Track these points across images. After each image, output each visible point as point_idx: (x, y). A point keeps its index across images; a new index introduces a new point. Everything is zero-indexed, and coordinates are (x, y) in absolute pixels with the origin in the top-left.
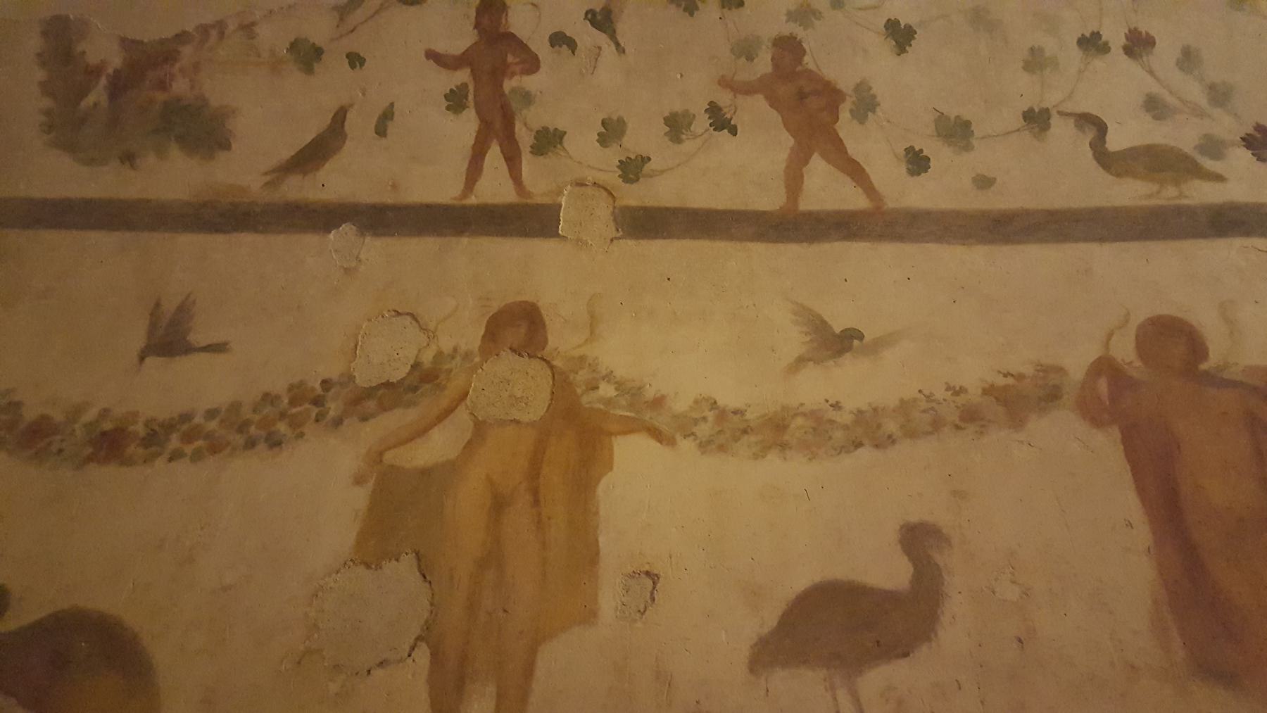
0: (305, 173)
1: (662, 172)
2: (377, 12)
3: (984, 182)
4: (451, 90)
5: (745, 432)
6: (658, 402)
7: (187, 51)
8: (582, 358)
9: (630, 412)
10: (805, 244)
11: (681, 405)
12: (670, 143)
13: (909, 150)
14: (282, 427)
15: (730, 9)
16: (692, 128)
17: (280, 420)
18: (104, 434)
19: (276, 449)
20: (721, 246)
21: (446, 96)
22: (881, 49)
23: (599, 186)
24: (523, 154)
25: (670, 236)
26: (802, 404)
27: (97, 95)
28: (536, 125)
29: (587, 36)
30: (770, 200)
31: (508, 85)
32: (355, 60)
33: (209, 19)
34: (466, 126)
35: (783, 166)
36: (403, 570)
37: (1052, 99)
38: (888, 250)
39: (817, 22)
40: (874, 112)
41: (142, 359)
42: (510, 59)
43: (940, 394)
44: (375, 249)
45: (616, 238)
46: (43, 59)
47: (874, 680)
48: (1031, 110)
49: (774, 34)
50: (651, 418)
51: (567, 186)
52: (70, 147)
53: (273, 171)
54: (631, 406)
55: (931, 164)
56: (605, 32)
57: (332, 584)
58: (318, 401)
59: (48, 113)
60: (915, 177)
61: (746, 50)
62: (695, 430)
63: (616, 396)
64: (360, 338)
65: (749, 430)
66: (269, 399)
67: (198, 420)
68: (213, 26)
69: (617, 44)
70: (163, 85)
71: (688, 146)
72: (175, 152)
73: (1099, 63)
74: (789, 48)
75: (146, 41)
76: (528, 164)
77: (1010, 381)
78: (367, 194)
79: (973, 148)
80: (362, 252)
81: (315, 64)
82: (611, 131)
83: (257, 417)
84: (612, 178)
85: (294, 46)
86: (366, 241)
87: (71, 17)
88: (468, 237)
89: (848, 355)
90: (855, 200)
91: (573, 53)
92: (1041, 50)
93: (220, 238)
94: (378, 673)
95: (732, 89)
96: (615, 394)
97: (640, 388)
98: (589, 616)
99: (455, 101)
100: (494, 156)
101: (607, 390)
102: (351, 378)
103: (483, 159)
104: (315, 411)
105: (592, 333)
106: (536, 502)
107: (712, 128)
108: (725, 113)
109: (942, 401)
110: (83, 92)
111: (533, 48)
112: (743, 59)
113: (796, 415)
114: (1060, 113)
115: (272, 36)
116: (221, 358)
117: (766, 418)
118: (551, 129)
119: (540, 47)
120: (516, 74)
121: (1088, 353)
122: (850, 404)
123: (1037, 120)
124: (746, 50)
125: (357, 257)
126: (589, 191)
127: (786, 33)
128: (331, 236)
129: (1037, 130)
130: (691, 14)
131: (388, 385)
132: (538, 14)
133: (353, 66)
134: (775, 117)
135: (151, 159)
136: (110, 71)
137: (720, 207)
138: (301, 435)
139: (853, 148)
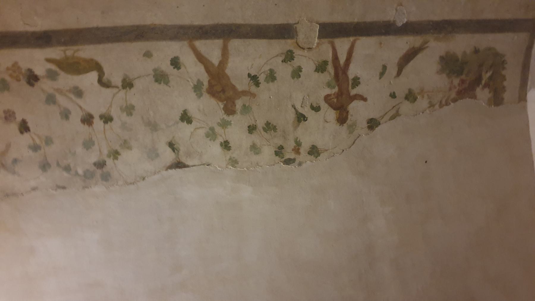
0: (413, 48)
1: (277, 56)
2: (384, 115)
3: (148, 55)
7: (453, 95)
10: (220, 23)
15: (253, 125)
16: (265, 76)
20: (254, 21)
22: (193, 111)
25: (275, 25)
27: (486, 76)
28: (326, 73)
29: (306, 111)
30: (235, 44)
31: (336, 90)
32: (393, 96)
33: (446, 108)
34: (353, 71)
35: (230, 60)
37: (122, 93)
38: (186, 21)
39: (219, 121)
40: (195, 85)
42: (335, 100)
46: (504, 89)
48: (130, 88)
49: (235, 116)
51: (315, 48)
52: (497, 55)
53: (425, 48)
55: (170, 62)
56: (300, 113)
60: (176, 56)
61: (246, 109)
68: (444, 105)
69: (295, 108)
70: (463, 82)
71: (267, 68)
72: (460, 55)
73: (103, 110)
74: (230, 110)
75: (467, 99)
76: (329, 57)
79: (153, 70)
82: (297, 73)
84: (297, 52)
85: (415, 99)
87: (493, 106)
90: (199, 44)
91: (312, 104)
99: (356, 82)
100: (342, 59)
108: (253, 83)
110: (490, 78)
111: (326, 105)
112: (247, 105)
115: (422, 103)
118: (320, 73)
119: (324, 106)
120: (333, 94)
123: (127, 84)
124: (246, 109)
126: (306, 46)
127: (231, 116)
128: (405, 20)
129: (127, 79)
130: (267, 122)
132: (325, 118)
133: (394, 93)
134: (233, 82)
135: (468, 52)
136: (481, 86)
137: (254, 40)
139: (201, 68)
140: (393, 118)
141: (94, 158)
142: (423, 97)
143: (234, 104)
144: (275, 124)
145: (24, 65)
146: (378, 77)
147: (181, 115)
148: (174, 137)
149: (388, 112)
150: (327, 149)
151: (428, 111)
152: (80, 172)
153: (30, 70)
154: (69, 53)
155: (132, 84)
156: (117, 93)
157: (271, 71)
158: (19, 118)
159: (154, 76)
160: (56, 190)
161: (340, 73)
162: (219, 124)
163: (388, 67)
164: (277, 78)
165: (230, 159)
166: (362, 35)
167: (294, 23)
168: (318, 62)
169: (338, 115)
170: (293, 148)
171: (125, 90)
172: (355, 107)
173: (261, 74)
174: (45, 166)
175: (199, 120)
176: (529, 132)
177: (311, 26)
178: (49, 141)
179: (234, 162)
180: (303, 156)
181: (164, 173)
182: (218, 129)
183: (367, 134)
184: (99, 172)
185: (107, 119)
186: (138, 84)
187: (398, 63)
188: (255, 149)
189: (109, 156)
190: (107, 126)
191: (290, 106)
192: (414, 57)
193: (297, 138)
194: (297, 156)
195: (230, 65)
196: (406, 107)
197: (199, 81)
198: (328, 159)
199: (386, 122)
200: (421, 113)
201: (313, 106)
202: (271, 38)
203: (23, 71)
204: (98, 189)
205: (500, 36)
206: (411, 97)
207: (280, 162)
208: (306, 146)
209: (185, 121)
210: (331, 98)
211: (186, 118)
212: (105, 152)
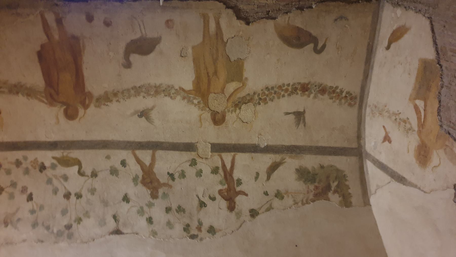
0: (275, 162)
1: (186, 161)
2: (261, 207)
3: (108, 157)
4: (240, 185)
5: (164, 91)
6: (184, 98)
7: (311, 196)
8: (202, 110)
9: (190, 96)
10: (151, 141)
11: (179, 98)
12: (184, 170)
13: (125, 167)
14: (267, 92)
15: (169, 207)
17: (268, 94)
18: (307, 91)
19: (266, 87)
20: (171, 141)
21: (242, 183)
23: (202, 158)
24: (221, 167)
25: (183, 143)
26: (151, 98)
27: (334, 185)
29: (206, 200)
30: (160, 153)
31: (226, 186)
32: (266, 194)
34: (236, 175)
36: (232, 59)
37: (90, 180)
38: (132, 139)
39: (147, 203)
41: (304, 111)
42: (226, 194)
43: (121, 100)
44: (255, 140)
45: (196, 143)
47: (138, 36)
50: (185, 94)
53: (284, 163)
54: (190, 97)
56: (202, 201)
57: (247, 55)
58: (260, 99)
59: (346, 180)
61: (165, 195)
62: (175, 91)
63: (193, 100)
64: (254, 116)
65: (163, 91)
66: (272, 100)
67: (286, 94)
68: (305, 204)
69: (198, 197)
70: (316, 188)
71: (179, 169)
72: (310, 169)
73: (78, 190)
74: (154, 196)
76: (220, 164)
77: (106, 104)
78: (258, 156)
80: (258, 140)
81: (277, 193)
83: (273, 95)
84: (199, 160)
85: (282, 198)
86: (257, 143)
87: (344, 207)
88: (232, 144)
89: (141, 111)
90: (138, 152)
92: (91, 194)
93: (293, 144)
94: (233, 36)
95: (169, 185)
97: (188, 102)
98: (193, 48)
100: (228, 167)
101: (196, 102)
102: (254, 105)
103: (231, 165)
104: (260, 96)
105: (200, 117)
106: (208, 73)
107: (174, 174)
109: (121, 98)
110: (338, 186)
111: (220, 197)
112: (166, 193)
113: (153, 95)
114: (88, 176)
115: (288, 201)
116: (286, 111)
117: (159, 94)
119: (218, 197)
120: (224, 189)
121: (89, 111)
122: (141, 97)
124: (165, 195)
125: (259, 138)
126: (204, 157)
127: (155, 200)
130: (179, 205)
131: (246, 103)
133: (267, 192)
134: (158, 177)
136: (331, 192)
137: (171, 151)
138: (262, 90)
139: (138, 168)
140: (268, 210)
142: (288, 196)
143: (157, 192)
144: (184, 207)
145: (40, 160)
146: (254, 180)
147: (123, 197)
148: (117, 212)
150: (221, 229)
152: (55, 231)
153: (43, 163)
154: (65, 154)
155: (97, 175)
156: (88, 179)
157: (183, 171)
158: (29, 192)
159: (110, 171)
160: (37, 243)
162: (147, 205)
163: (260, 173)
164: (186, 176)
165: (152, 231)
166: (239, 152)
167: (195, 142)
168: (212, 167)
169: (228, 204)
170: (197, 226)
171: (92, 178)
172: (239, 199)
173: (176, 172)
174: (35, 225)
175: (134, 201)
176: (378, 229)
177: (206, 145)
178: (41, 208)
179: (154, 233)
180: (204, 233)
181: (108, 237)
182: (146, 208)
183: (250, 221)
184: (67, 232)
185: (79, 196)
186: (100, 175)
187: (267, 171)
188: (169, 224)
189: (75, 221)
190: (78, 201)
191: (195, 196)
192: (277, 168)
193: (200, 219)
194: (199, 233)
195: (156, 166)
196: (276, 203)
197: (136, 175)
198: (221, 237)
199: (263, 213)
200: (289, 208)
201: (211, 197)
202: (182, 150)
203: (39, 163)
204: (63, 244)
207: (187, 237)
209: (125, 202)
210: (223, 192)
211: (126, 199)
212: (73, 218)
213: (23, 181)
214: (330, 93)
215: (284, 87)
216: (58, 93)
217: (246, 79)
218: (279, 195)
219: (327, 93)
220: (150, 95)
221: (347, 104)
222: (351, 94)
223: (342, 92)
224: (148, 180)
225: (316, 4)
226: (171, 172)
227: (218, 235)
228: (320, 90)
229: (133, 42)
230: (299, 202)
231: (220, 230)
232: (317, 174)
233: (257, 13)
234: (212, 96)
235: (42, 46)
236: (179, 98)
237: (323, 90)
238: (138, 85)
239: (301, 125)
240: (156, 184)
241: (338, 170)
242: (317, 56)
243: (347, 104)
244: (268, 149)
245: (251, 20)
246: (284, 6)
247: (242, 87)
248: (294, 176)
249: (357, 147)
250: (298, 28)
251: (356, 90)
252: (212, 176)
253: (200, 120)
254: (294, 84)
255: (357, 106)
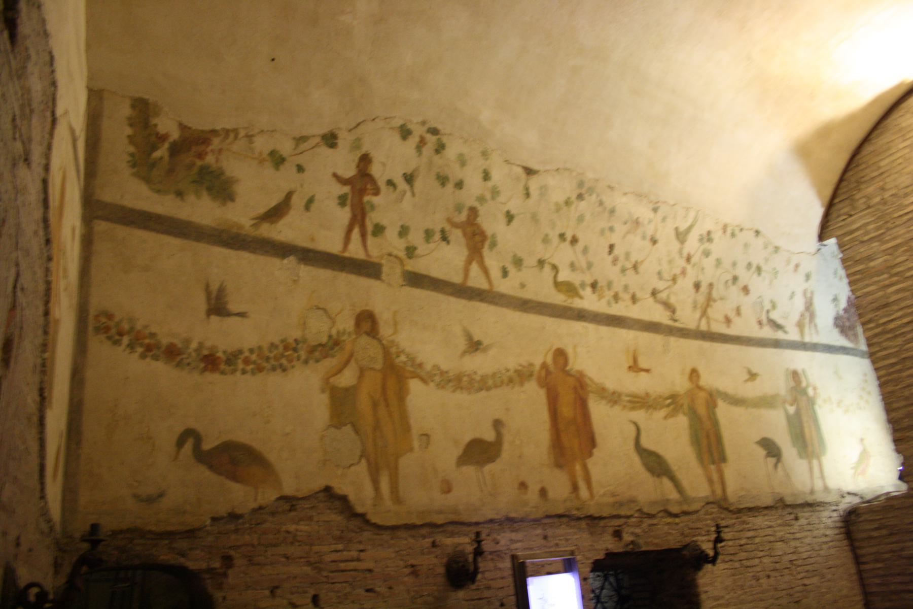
0: (272, 222)
1: (423, 256)
6: (420, 365)
7: (216, 142)
11: (428, 367)
13: (503, 266)
14: (284, 361)
18: (206, 356)
22: (502, 219)
27: (162, 152)
29: (402, 185)
30: (457, 279)
31: (366, 198)
32: (300, 169)
34: (344, 215)
36: (348, 429)
37: (547, 256)
38: (492, 308)
42: (369, 186)
44: (307, 272)
47: (488, 468)
54: (412, 366)
58: (295, 350)
59: (132, 155)
61: (459, 208)
66: (273, 346)
67: (247, 354)
70: (200, 156)
74: (473, 212)
76: (370, 240)
78: (302, 241)
82: (404, 231)
84: (402, 254)
85: (273, 153)
89: (478, 351)
96: (406, 360)
98: (411, 449)
100: (356, 233)
101: (403, 358)
110: (154, 148)
113: (465, 376)
115: (262, 145)
119: (382, 184)
122: (480, 373)
124: (459, 208)
127: (475, 205)
131: (320, 345)
138: (293, 367)
141: (583, 204)
143: (469, 217)
145: (594, 297)
146: (316, 198)
149: (308, 150)
151: (256, 131)
161: (359, 217)
165: (487, 159)
172: (349, 172)
180: (418, 131)
182: (488, 196)
192: (269, 211)
196: (286, 147)
205: (129, 202)
206: (278, 160)
208: (413, 141)
211: (510, 217)
212: (573, 207)
213: (612, 273)
214: (158, 346)
215: (252, 369)
216: (575, 388)
217: (323, 391)
218: (278, 160)
219: (163, 348)
220: (469, 375)
221: (117, 319)
222: (109, 338)
223: (131, 346)
224: (478, 238)
225: (205, 526)
226: (444, 243)
227: (398, 122)
228: (178, 355)
229: (492, 459)
230: (243, 137)
231: (392, 128)
232: (194, 182)
233: (312, 508)
234: (379, 366)
235: (590, 455)
236: (428, 367)
237: (172, 353)
238: (483, 393)
239: (214, 287)
240: (469, 230)
241: (147, 180)
242: (192, 424)
243: (117, 319)
244: (283, 250)
245: (321, 496)
246: (265, 521)
247: (331, 377)
248: (242, 190)
249: (96, 221)
250: (235, 478)
251: (98, 347)
252: (384, 222)
253: (395, 324)
254: (234, 372)
255: (92, 312)
